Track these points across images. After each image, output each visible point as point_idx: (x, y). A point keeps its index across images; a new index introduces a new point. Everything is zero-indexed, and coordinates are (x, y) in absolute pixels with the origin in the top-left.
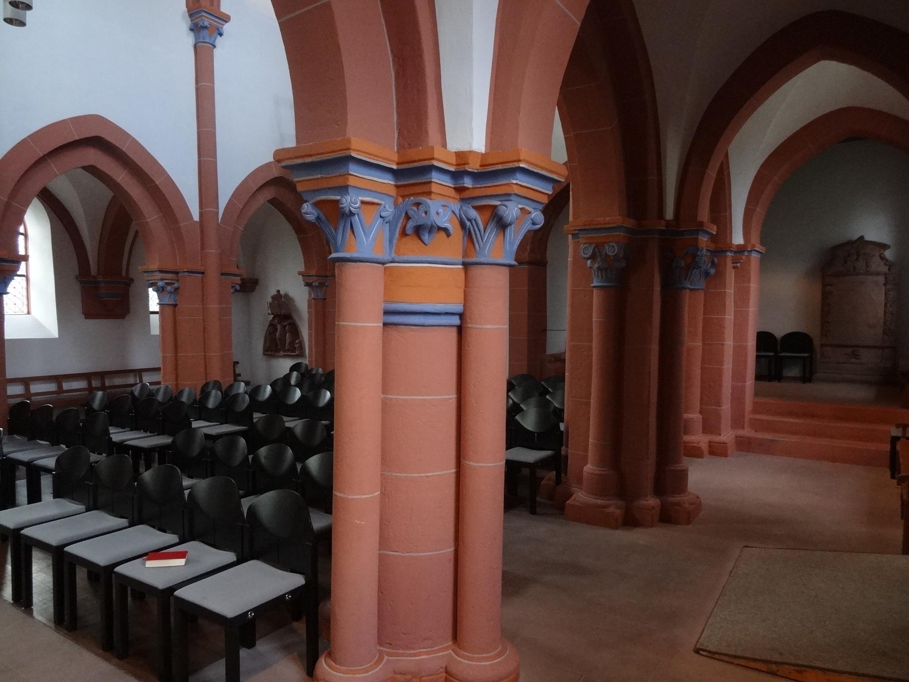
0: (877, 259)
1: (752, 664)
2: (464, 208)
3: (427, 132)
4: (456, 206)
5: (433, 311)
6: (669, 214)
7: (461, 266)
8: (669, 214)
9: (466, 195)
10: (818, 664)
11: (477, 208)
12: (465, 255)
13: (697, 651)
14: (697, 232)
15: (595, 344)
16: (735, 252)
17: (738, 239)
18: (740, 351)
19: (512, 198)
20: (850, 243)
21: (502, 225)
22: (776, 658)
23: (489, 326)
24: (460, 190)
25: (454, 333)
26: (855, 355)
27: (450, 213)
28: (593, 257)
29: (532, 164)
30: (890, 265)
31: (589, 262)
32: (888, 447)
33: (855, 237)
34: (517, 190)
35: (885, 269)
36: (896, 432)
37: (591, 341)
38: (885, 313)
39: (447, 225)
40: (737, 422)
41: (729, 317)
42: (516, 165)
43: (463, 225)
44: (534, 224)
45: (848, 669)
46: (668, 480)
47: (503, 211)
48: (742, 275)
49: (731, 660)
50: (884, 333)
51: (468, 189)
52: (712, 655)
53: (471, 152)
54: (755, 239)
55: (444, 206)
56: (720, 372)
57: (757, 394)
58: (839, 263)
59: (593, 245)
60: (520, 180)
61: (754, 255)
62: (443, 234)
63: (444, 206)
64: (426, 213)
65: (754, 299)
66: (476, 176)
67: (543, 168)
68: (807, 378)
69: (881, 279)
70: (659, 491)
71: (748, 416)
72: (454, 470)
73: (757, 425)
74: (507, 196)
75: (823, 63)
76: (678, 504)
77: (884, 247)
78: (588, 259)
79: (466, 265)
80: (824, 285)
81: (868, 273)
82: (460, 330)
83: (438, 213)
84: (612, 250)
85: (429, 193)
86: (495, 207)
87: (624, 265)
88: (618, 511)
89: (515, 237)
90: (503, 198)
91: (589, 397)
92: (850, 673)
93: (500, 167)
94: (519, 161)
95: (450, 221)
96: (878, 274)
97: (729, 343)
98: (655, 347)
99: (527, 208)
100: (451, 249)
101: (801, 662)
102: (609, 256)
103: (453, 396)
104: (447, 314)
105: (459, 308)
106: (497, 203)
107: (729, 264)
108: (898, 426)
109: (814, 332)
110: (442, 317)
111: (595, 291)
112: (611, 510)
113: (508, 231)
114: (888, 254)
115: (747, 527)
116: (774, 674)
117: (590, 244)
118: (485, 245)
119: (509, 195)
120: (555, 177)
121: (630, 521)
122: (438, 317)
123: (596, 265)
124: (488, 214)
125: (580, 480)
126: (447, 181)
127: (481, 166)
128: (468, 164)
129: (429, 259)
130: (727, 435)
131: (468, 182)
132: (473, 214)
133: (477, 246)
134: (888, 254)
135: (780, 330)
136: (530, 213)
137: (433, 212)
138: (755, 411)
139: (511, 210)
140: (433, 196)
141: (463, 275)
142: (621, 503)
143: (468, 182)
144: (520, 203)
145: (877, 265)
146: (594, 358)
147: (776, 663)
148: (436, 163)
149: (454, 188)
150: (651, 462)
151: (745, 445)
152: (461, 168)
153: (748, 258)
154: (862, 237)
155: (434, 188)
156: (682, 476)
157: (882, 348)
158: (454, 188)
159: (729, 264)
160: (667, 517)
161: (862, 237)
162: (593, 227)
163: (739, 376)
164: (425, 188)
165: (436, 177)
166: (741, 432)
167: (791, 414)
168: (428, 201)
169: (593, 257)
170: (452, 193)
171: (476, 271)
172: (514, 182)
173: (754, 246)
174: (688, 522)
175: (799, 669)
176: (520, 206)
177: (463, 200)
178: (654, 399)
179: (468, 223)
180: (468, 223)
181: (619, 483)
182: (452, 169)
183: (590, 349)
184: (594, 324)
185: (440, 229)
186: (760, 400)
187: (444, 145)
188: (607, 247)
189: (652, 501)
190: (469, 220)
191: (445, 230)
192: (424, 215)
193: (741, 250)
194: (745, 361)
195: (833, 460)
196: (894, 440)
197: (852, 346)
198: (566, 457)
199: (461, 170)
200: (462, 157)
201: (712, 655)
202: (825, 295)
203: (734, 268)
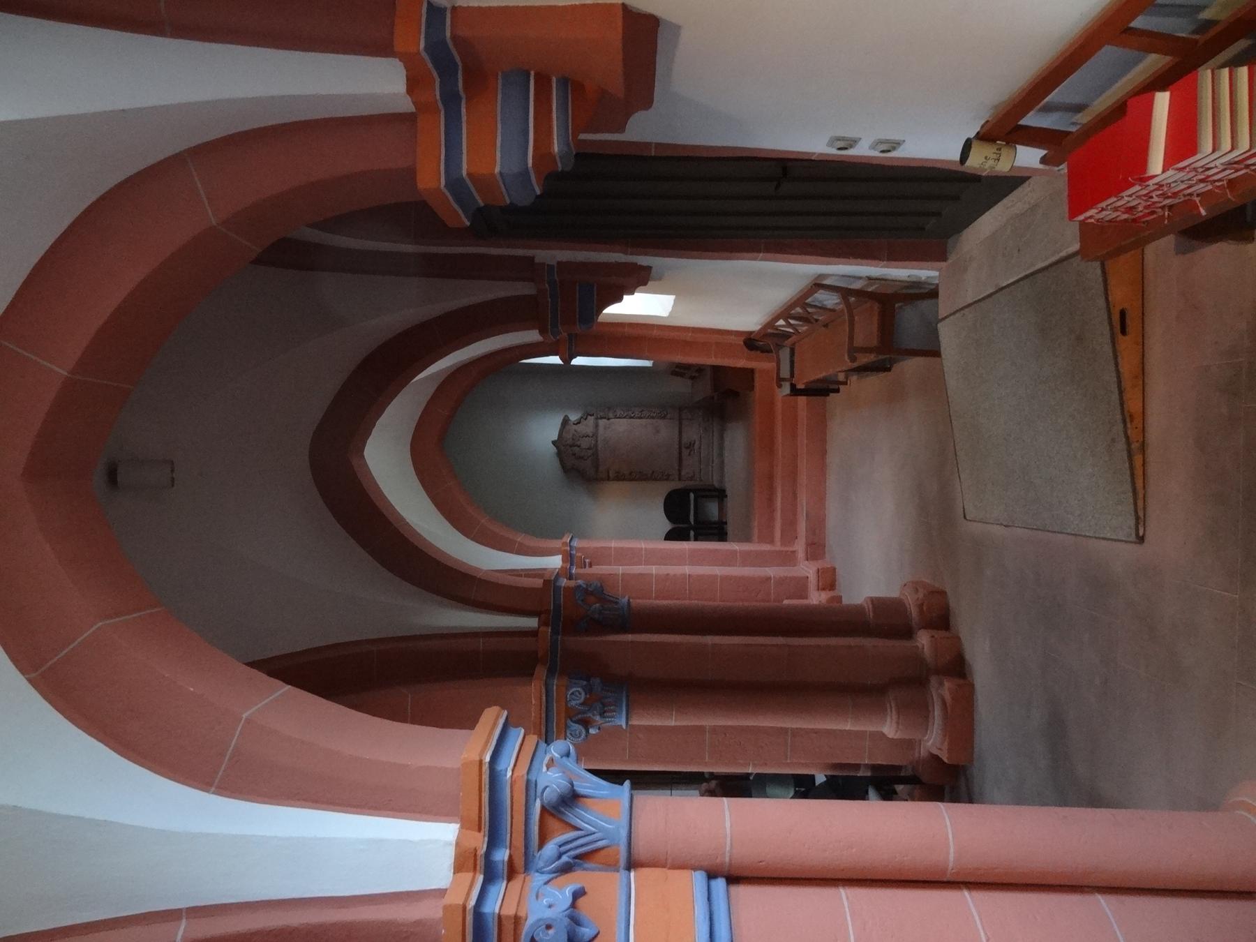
0: (579, 428)
1: (1139, 472)
2: (541, 864)
3: (418, 923)
4: (537, 880)
5: (707, 923)
6: (531, 623)
7: (632, 874)
8: (531, 623)
9: (519, 862)
10: (1115, 397)
11: (543, 841)
12: (611, 866)
13: (1141, 540)
14: (557, 589)
15: (710, 721)
16: (572, 564)
17: (555, 562)
18: (695, 559)
19: (533, 777)
20: (559, 454)
21: (571, 798)
22: (1121, 445)
23: (728, 825)
24: (512, 873)
25: (741, 891)
26: (690, 446)
27: (548, 888)
28: (586, 724)
29: (487, 742)
30: (587, 415)
31: (592, 731)
32: (802, 400)
33: (553, 449)
34: (522, 770)
35: (591, 420)
36: (786, 389)
37: (701, 729)
38: (640, 418)
39: (568, 892)
40: (787, 558)
41: (654, 570)
42: (486, 768)
43: (566, 869)
44: (568, 755)
45: (1112, 368)
46: (886, 621)
47: (551, 795)
48: (598, 557)
49: (1141, 496)
50: (664, 418)
51: (510, 856)
52: (1140, 520)
53: (457, 844)
54: (557, 544)
55: (537, 897)
56: (725, 579)
57: (747, 539)
58: (583, 466)
59: (569, 722)
60: (507, 765)
61: (575, 543)
62: (581, 902)
63: (537, 897)
64: (549, 927)
65: (628, 543)
66: (494, 840)
67: (495, 724)
68: (720, 494)
69: (602, 422)
70: (907, 633)
71: (778, 547)
72: (966, 893)
73: (790, 534)
74: (529, 786)
75: (365, 453)
76: (920, 606)
77: (566, 422)
78: (587, 731)
79: (632, 865)
80: (609, 479)
81: (595, 435)
82: (734, 879)
83: (550, 906)
84: (576, 695)
85: (517, 921)
86: (543, 809)
87: (598, 680)
88: (947, 684)
89: (589, 785)
90: (532, 793)
91: (785, 731)
92: (1117, 365)
93: (486, 796)
94: (481, 762)
95: (561, 888)
96: (597, 426)
97: (687, 570)
98: (709, 640)
99: (546, 761)
100: (609, 890)
101: (1119, 417)
102: (586, 699)
103: (843, 893)
104: (709, 899)
105: (699, 877)
106: (538, 804)
107: (587, 570)
108: (780, 386)
109: (664, 488)
110: (715, 908)
111: (635, 722)
112: (948, 697)
113: (581, 790)
114: (574, 417)
115: (936, 521)
116: (1143, 448)
117: (566, 727)
118: (601, 829)
119: (528, 782)
120: (501, 721)
121: (958, 668)
122: (715, 917)
123: (598, 718)
124: (553, 823)
125: (909, 744)
126: (498, 891)
127: (479, 830)
128: (476, 850)
129: (623, 926)
130: (807, 570)
131: (502, 855)
132: (550, 848)
133: (600, 844)
134: (574, 417)
135: (667, 526)
136: (552, 760)
137: (549, 914)
138: (772, 542)
139: (551, 781)
140: (522, 914)
141: (645, 871)
142: (934, 680)
143: (502, 855)
144: (540, 769)
145: (588, 427)
146: (730, 723)
147: (1128, 443)
148: (472, 903)
149: (509, 879)
150: (868, 643)
151: (816, 549)
152: (481, 863)
153: (578, 549)
154: (554, 443)
155: (509, 911)
156: (878, 604)
157: (681, 424)
158: (509, 879)
159: (587, 570)
160: (940, 619)
161: (554, 443)
162: (544, 721)
163: (729, 559)
164: (509, 927)
165: (492, 906)
166: (801, 555)
167: (771, 501)
168: (530, 921)
169: (586, 724)
170: (516, 884)
171: (642, 849)
172: (509, 774)
173: (564, 544)
174: (942, 593)
175: (1128, 420)
176: (545, 769)
177: (527, 868)
178: (780, 640)
179: (565, 858)
180: (565, 858)
181: (906, 685)
182: (480, 878)
183: (714, 730)
184: (678, 724)
185: (573, 905)
186: (755, 538)
187: (441, 893)
188: (573, 703)
189: (924, 640)
190: (559, 857)
191: (578, 895)
192: (551, 932)
193: (569, 558)
194: (710, 551)
195: (824, 453)
196: (795, 391)
197: (680, 448)
198: (874, 768)
199: (481, 864)
200: (463, 862)
201: (1140, 520)
202: (620, 477)
203: (591, 565)
